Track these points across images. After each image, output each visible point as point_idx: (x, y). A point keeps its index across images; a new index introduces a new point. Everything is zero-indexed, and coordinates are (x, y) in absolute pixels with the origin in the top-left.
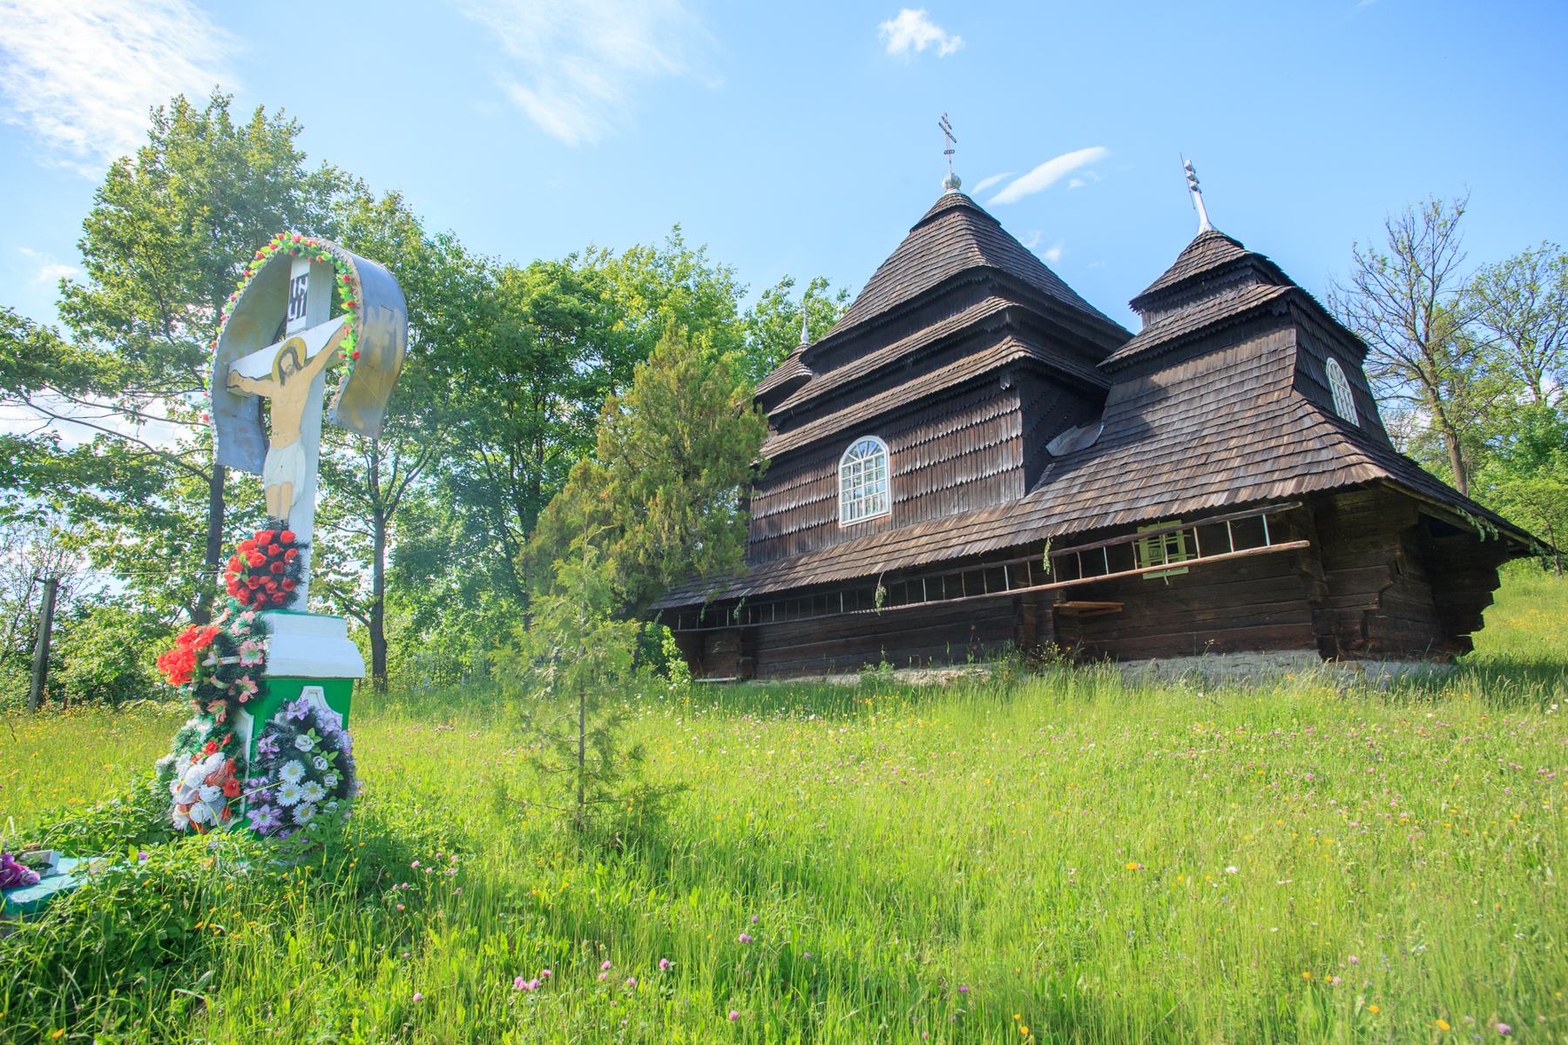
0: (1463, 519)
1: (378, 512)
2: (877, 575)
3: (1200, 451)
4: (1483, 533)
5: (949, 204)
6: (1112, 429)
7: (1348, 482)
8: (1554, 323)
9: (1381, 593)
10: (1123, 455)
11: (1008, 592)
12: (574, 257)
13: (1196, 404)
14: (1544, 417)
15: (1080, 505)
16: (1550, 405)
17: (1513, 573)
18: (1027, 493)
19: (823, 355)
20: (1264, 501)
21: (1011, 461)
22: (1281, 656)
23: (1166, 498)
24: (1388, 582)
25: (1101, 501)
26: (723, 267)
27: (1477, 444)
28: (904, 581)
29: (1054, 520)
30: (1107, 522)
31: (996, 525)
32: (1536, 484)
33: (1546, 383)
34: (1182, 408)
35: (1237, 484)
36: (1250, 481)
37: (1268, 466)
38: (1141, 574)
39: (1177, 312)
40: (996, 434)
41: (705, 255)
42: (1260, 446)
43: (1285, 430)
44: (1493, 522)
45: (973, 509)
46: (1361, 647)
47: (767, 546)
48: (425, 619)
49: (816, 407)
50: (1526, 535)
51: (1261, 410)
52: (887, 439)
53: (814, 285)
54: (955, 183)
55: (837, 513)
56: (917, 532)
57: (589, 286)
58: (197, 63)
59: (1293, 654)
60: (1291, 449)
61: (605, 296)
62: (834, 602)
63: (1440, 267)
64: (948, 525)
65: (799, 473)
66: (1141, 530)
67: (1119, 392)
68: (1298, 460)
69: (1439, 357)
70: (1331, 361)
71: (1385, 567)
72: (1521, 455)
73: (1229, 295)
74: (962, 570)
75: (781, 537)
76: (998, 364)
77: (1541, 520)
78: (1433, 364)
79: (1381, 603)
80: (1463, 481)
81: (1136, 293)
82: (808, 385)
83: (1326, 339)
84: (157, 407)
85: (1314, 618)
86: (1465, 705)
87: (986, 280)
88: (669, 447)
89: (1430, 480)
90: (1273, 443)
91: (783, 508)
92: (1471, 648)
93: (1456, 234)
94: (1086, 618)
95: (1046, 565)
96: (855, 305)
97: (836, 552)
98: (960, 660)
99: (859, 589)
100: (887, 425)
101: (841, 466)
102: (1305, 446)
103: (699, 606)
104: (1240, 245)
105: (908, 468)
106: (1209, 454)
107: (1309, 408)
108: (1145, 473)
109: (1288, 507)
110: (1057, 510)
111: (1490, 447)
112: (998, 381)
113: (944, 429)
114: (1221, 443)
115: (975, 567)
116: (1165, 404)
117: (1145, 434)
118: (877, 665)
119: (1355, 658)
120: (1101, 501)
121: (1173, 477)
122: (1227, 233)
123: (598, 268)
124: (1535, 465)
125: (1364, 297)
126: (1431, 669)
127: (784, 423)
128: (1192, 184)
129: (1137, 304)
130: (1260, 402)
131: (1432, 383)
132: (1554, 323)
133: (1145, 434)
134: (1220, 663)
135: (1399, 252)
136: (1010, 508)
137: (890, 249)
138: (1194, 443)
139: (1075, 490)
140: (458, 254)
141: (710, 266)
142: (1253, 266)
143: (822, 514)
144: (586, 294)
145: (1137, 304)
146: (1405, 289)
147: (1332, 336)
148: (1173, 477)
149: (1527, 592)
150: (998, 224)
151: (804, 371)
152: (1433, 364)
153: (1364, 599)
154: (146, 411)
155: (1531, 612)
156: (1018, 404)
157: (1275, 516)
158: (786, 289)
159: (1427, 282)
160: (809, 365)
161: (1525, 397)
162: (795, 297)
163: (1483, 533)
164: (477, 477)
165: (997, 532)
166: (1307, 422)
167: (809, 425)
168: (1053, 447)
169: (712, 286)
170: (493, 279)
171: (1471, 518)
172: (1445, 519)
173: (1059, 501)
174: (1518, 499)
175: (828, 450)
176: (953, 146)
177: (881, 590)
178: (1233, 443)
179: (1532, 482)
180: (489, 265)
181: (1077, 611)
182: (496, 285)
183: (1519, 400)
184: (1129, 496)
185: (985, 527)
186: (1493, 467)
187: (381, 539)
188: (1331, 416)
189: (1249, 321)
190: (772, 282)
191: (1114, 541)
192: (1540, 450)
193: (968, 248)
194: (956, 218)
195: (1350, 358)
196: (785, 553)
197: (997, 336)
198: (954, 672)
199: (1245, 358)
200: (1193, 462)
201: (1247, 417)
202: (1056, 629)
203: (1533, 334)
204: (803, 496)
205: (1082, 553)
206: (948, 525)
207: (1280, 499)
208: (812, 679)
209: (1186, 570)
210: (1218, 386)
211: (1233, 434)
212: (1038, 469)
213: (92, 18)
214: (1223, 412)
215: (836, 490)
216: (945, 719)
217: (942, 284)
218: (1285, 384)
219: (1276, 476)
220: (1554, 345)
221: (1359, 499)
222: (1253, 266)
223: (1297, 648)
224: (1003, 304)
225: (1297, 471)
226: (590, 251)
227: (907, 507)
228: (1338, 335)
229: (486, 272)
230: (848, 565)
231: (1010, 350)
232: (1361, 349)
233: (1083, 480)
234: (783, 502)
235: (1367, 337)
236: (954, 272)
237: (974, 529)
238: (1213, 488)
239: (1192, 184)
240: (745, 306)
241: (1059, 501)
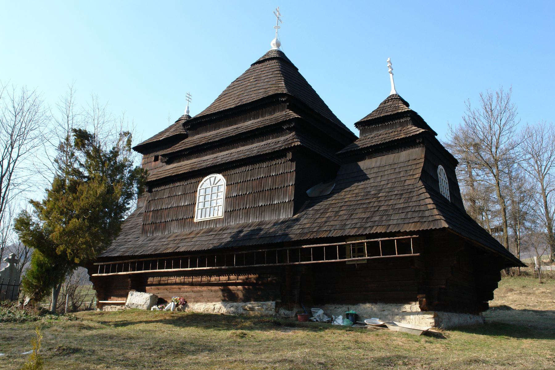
21: (289, 197)
70: (440, 167)
81: (358, 120)
104: (407, 105)
127: (171, 159)
129: (357, 125)
145: (357, 125)
150: (298, 69)
155: (509, 295)
156: (294, 169)
194: (274, 63)
209: (365, 262)
224: (293, 115)
231: (288, 139)
232: (455, 163)
236: (271, 93)
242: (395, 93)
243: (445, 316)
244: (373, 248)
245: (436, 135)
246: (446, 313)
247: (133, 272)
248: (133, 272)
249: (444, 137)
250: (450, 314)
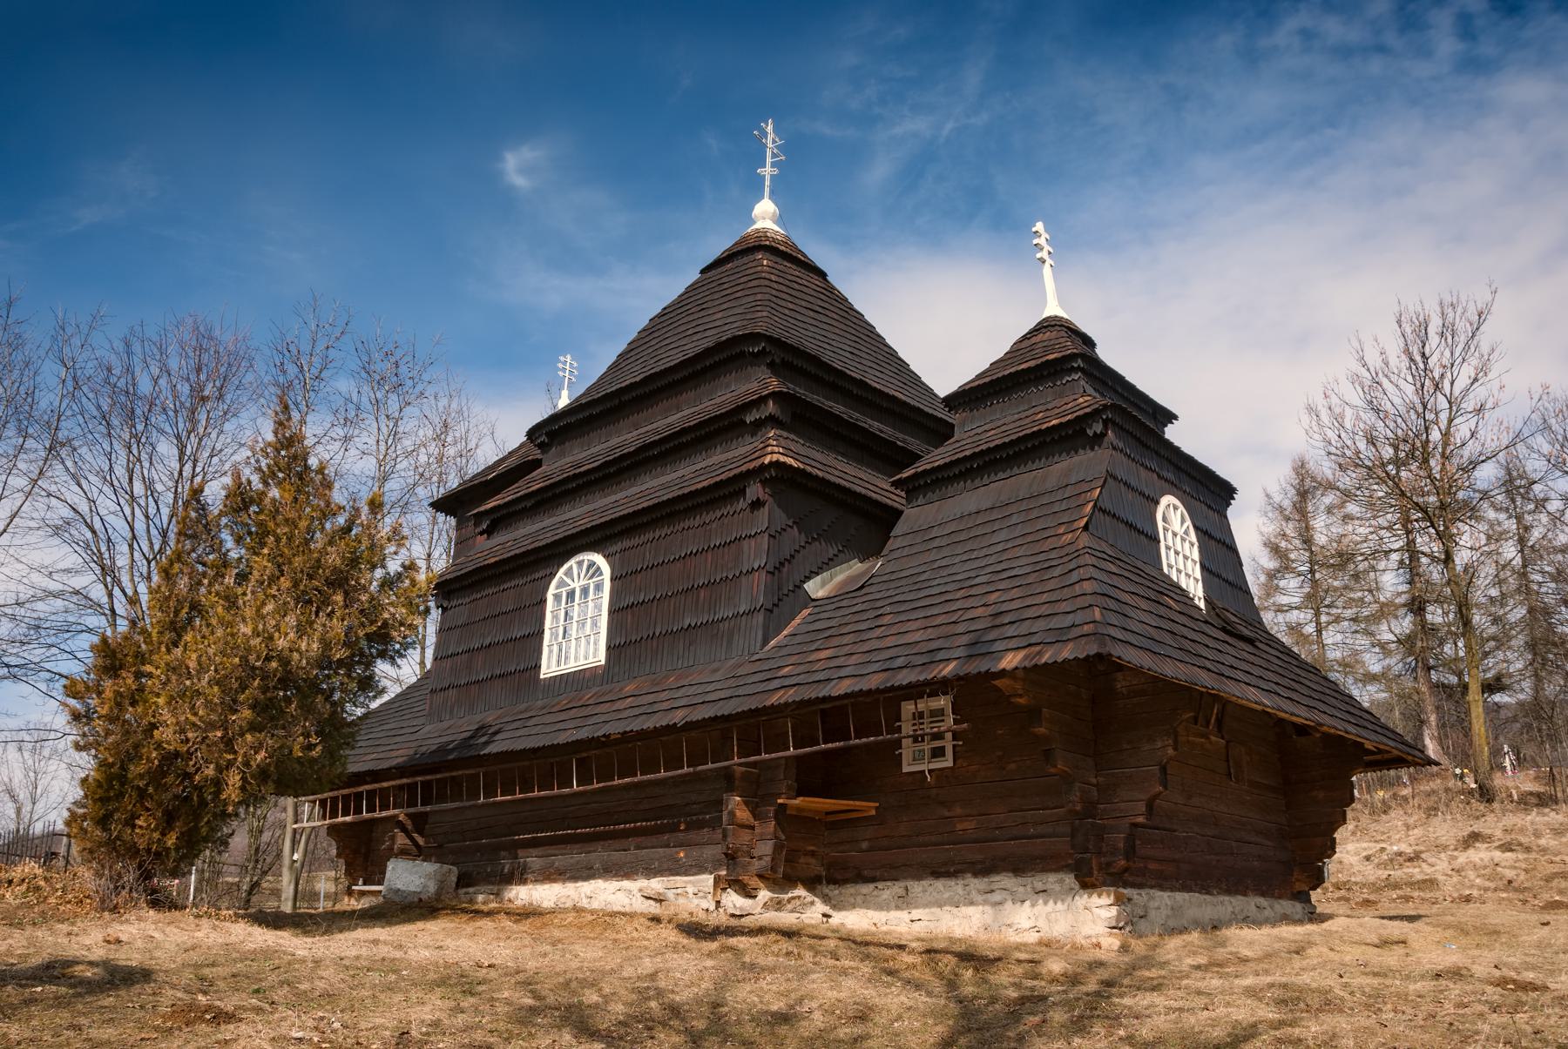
87: (763, 352)
150: (822, 275)
224: (774, 384)
243: (1161, 901)
245: (1170, 417)
246: (1166, 895)
250: (1180, 897)
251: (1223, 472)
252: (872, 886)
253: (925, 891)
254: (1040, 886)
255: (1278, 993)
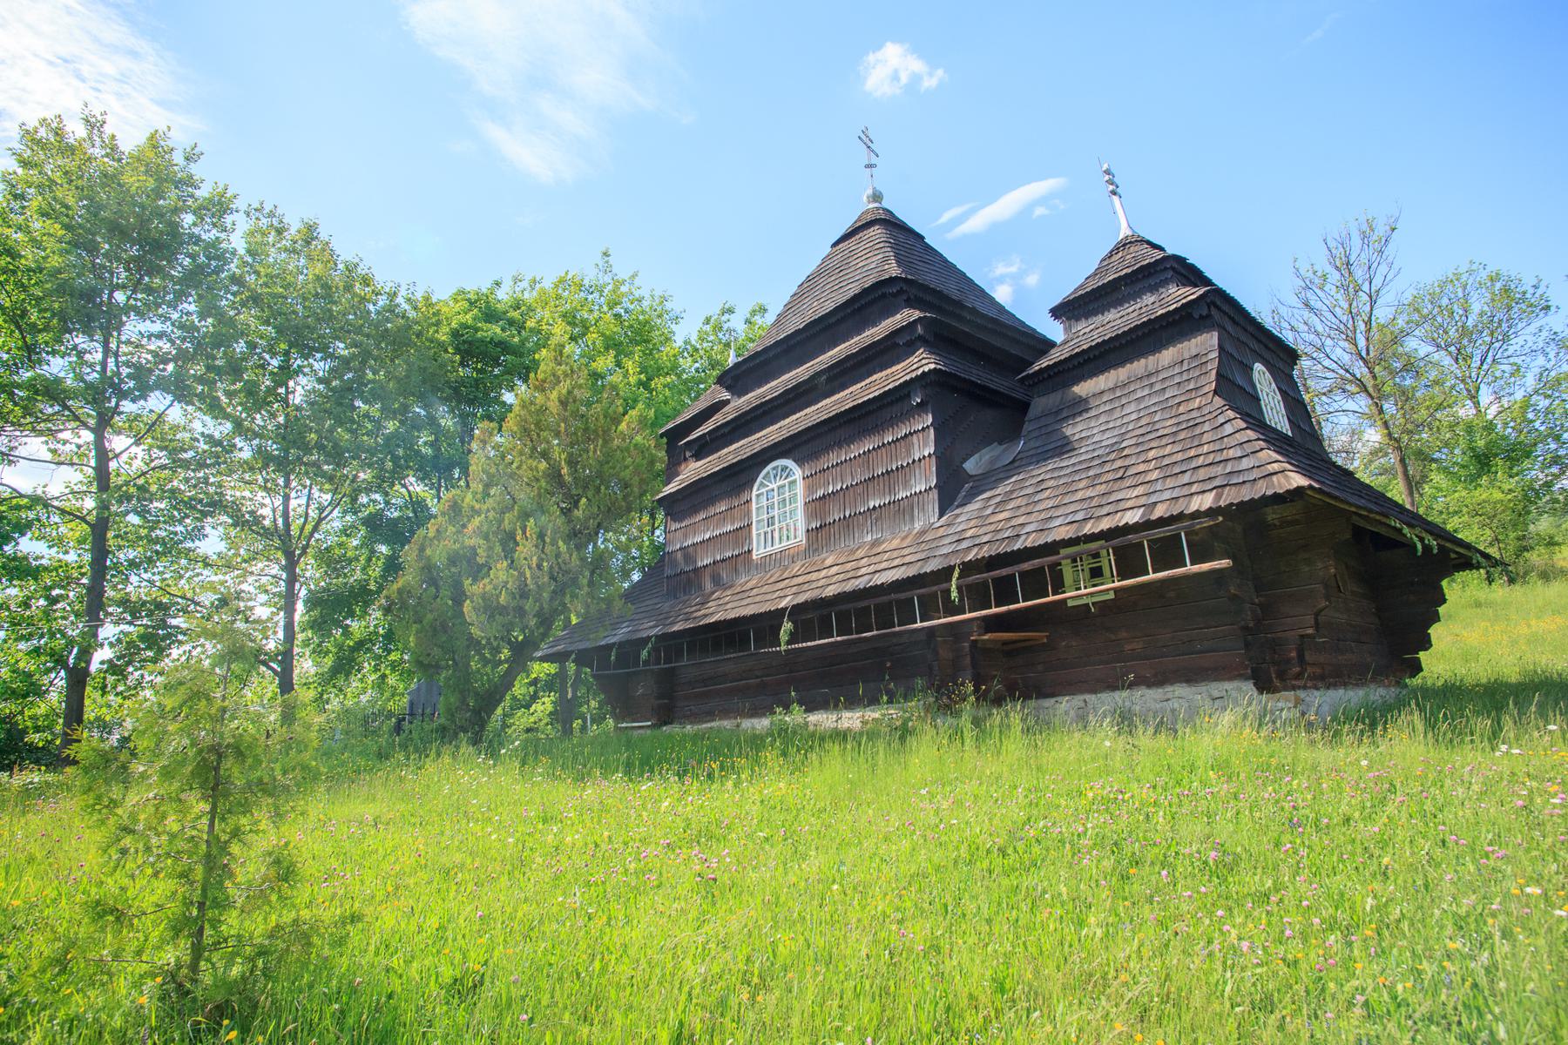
0: (1400, 531)
1: (289, 555)
2: (784, 609)
3: (1119, 463)
4: (1419, 546)
5: (869, 218)
6: (1033, 444)
7: (1270, 492)
8: (1488, 339)
9: (1317, 615)
10: (1041, 471)
11: (919, 625)
12: (498, 284)
13: (1117, 414)
14: (1485, 428)
15: (992, 528)
16: (1489, 417)
17: (1464, 585)
18: (941, 515)
19: (737, 378)
20: (1181, 516)
21: (924, 481)
22: (1217, 688)
23: (1080, 516)
24: (1324, 603)
25: (1013, 522)
26: (657, 293)
27: (1424, 457)
28: (815, 615)
29: (964, 545)
30: (1018, 546)
31: (906, 551)
32: (1481, 494)
33: (1485, 397)
34: (1103, 419)
35: (1153, 499)
36: (1167, 495)
37: (1186, 478)
38: (1064, 601)
39: (1098, 319)
40: (909, 453)
41: (637, 282)
42: (1180, 457)
43: (1206, 438)
44: (1431, 533)
45: (887, 535)
46: (1298, 676)
47: (672, 577)
48: (345, 666)
49: (734, 430)
50: (1468, 546)
51: (1182, 418)
52: (800, 462)
53: (753, 313)
54: (877, 197)
55: (750, 543)
56: (829, 562)
57: (515, 315)
58: (161, 103)
59: (1228, 685)
60: (1210, 459)
61: (530, 324)
62: (744, 642)
63: (1377, 282)
64: (860, 553)
65: (712, 501)
66: (1064, 552)
67: (1040, 404)
68: (1219, 470)
69: (1382, 372)
70: (1258, 367)
71: (1319, 587)
72: (1463, 467)
73: (1149, 299)
74: (871, 603)
75: (696, 570)
76: (913, 375)
77: (1488, 532)
78: (1375, 377)
79: (1317, 626)
80: (1411, 494)
82: (726, 409)
83: (1253, 344)
84: (34, 446)
85: (1247, 645)
86: (1406, 747)
87: (901, 292)
88: (546, 475)
89: (1378, 497)
90: (1192, 453)
91: (698, 539)
92: (1420, 669)
93: (1390, 250)
94: (1010, 651)
95: (954, 594)
96: (778, 321)
97: (750, 585)
98: (873, 701)
99: (766, 624)
100: (799, 447)
101: (755, 492)
102: (1225, 455)
103: (609, 647)
104: (1161, 249)
105: (820, 493)
106: (1127, 467)
107: (1231, 414)
108: (1061, 490)
109: (1207, 523)
110: (969, 534)
111: (1434, 460)
112: (908, 396)
113: (857, 449)
114: (1144, 458)
115: (884, 599)
116: (1086, 415)
117: (1064, 447)
118: (787, 707)
119: (1294, 688)
120: (1013, 522)
121: (1089, 493)
122: (1148, 237)
123: (527, 295)
124: (1480, 476)
125: (1306, 314)
126: (1377, 693)
128: (1111, 188)
129: (1057, 312)
130: (1182, 409)
131: (1377, 397)
132: (1488, 339)
133: (1064, 447)
134: (1144, 698)
135: (1337, 268)
136: (923, 532)
137: (811, 267)
138: (1113, 456)
139: (989, 511)
140: (366, 281)
141: (645, 292)
142: (1173, 269)
143: (736, 544)
144: (511, 322)
145: (1057, 312)
146: (1345, 305)
147: (1259, 341)
148: (1089, 493)
149: (1478, 605)
150: (922, 238)
151: (726, 395)
152: (1375, 377)
153: (1298, 622)
154: (21, 451)
155: (1472, 633)
157: (1196, 533)
158: (727, 316)
159: (1364, 297)
160: (728, 388)
161: (1465, 411)
162: (737, 323)
163: (1419, 546)
164: (396, 514)
165: (907, 560)
166: (1228, 429)
167: (726, 451)
168: (971, 466)
169: (643, 312)
170: (407, 307)
171: (1406, 530)
172: (1383, 531)
173: (972, 523)
174: (1465, 510)
175: (739, 477)
176: (874, 160)
177: (787, 626)
178: (1151, 454)
179: (1477, 493)
180: (403, 292)
181: (1006, 644)
182: (412, 314)
183: (1462, 413)
184: (1043, 516)
185: (895, 554)
186: (1437, 478)
187: (292, 580)
188: (1255, 421)
189: (1170, 325)
190: (714, 311)
191: (1026, 566)
192: (1483, 462)
193: (885, 260)
195: (1281, 365)
196: (700, 588)
197: (910, 349)
198: (873, 714)
199: (1166, 363)
200: (1111, 476)
201: (1167, 426)
202: (974, 665)
203: (1469, 350)
204: (717, 526)
205: (1023, 574)
206: (860, 553)
207: (1197, 515)
208: (727, 724)
209: (1111, 596)
210: (1139, 394)
211: (1153, 444)
212: (953, 488)
213: (53, 59)
214: (1143, 422)
215: (750, 518)
216: (828, 774)
217: (855, 298)
218: (1206, 389)
219: (1194, 488)
220: (1489, 360)
221: (1288, 511)
222: (1173, 269)
223: (1230, 679)
224: (917, 314)
225: (1217, 483)
226: (516, 280)
227: (820, 535)
228: (1264, 339)
229: (400, 300)
230: (758, 599)
231: (922, 362)
232: (1292, 356)
233: (998, 499)
234: (699, 534)
235: (1301, 348)
237: (882, 557)
238: (1129, 504)
239: (1111, 188)
240: (685, 332)
241: (972, 523)
242: (1129, 233)
244: (1129, 563)
247: (984, 612)
248: (984, 612)
249: (1265, 295)
251: (1288, 337)
252: (1053, 700)
253: (219, 207)
254: (1216, 694)
255: (66, 220)
